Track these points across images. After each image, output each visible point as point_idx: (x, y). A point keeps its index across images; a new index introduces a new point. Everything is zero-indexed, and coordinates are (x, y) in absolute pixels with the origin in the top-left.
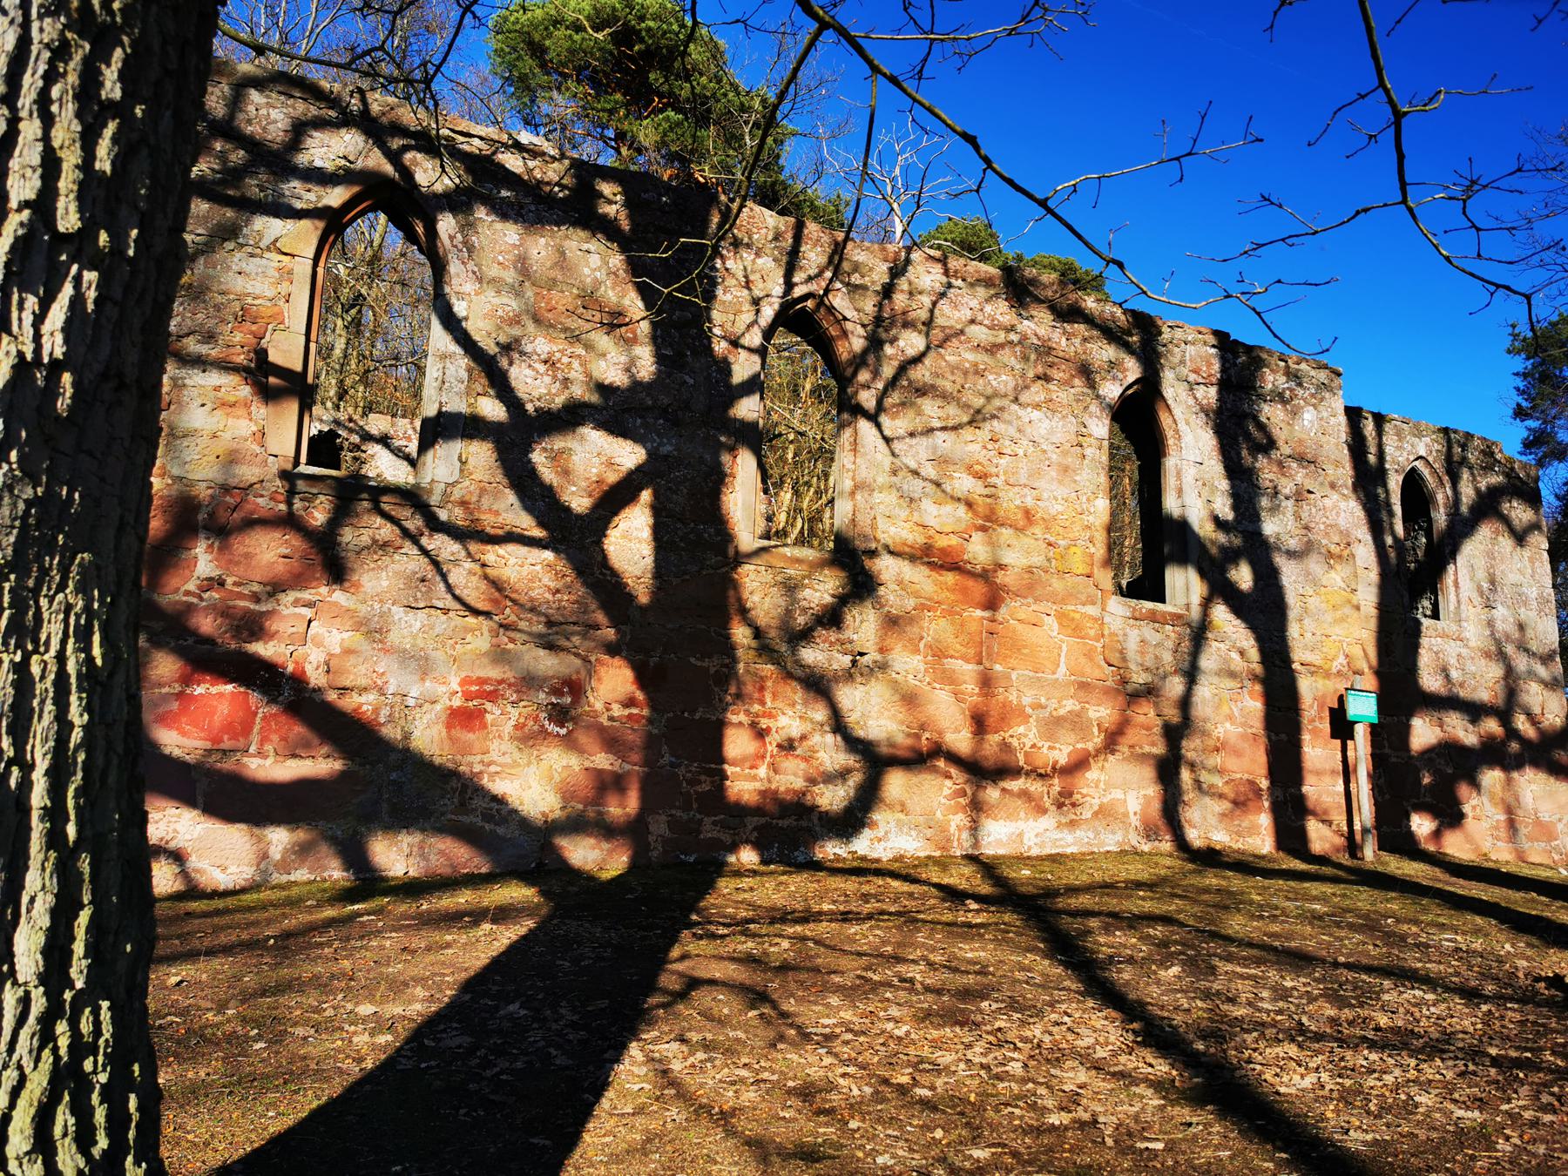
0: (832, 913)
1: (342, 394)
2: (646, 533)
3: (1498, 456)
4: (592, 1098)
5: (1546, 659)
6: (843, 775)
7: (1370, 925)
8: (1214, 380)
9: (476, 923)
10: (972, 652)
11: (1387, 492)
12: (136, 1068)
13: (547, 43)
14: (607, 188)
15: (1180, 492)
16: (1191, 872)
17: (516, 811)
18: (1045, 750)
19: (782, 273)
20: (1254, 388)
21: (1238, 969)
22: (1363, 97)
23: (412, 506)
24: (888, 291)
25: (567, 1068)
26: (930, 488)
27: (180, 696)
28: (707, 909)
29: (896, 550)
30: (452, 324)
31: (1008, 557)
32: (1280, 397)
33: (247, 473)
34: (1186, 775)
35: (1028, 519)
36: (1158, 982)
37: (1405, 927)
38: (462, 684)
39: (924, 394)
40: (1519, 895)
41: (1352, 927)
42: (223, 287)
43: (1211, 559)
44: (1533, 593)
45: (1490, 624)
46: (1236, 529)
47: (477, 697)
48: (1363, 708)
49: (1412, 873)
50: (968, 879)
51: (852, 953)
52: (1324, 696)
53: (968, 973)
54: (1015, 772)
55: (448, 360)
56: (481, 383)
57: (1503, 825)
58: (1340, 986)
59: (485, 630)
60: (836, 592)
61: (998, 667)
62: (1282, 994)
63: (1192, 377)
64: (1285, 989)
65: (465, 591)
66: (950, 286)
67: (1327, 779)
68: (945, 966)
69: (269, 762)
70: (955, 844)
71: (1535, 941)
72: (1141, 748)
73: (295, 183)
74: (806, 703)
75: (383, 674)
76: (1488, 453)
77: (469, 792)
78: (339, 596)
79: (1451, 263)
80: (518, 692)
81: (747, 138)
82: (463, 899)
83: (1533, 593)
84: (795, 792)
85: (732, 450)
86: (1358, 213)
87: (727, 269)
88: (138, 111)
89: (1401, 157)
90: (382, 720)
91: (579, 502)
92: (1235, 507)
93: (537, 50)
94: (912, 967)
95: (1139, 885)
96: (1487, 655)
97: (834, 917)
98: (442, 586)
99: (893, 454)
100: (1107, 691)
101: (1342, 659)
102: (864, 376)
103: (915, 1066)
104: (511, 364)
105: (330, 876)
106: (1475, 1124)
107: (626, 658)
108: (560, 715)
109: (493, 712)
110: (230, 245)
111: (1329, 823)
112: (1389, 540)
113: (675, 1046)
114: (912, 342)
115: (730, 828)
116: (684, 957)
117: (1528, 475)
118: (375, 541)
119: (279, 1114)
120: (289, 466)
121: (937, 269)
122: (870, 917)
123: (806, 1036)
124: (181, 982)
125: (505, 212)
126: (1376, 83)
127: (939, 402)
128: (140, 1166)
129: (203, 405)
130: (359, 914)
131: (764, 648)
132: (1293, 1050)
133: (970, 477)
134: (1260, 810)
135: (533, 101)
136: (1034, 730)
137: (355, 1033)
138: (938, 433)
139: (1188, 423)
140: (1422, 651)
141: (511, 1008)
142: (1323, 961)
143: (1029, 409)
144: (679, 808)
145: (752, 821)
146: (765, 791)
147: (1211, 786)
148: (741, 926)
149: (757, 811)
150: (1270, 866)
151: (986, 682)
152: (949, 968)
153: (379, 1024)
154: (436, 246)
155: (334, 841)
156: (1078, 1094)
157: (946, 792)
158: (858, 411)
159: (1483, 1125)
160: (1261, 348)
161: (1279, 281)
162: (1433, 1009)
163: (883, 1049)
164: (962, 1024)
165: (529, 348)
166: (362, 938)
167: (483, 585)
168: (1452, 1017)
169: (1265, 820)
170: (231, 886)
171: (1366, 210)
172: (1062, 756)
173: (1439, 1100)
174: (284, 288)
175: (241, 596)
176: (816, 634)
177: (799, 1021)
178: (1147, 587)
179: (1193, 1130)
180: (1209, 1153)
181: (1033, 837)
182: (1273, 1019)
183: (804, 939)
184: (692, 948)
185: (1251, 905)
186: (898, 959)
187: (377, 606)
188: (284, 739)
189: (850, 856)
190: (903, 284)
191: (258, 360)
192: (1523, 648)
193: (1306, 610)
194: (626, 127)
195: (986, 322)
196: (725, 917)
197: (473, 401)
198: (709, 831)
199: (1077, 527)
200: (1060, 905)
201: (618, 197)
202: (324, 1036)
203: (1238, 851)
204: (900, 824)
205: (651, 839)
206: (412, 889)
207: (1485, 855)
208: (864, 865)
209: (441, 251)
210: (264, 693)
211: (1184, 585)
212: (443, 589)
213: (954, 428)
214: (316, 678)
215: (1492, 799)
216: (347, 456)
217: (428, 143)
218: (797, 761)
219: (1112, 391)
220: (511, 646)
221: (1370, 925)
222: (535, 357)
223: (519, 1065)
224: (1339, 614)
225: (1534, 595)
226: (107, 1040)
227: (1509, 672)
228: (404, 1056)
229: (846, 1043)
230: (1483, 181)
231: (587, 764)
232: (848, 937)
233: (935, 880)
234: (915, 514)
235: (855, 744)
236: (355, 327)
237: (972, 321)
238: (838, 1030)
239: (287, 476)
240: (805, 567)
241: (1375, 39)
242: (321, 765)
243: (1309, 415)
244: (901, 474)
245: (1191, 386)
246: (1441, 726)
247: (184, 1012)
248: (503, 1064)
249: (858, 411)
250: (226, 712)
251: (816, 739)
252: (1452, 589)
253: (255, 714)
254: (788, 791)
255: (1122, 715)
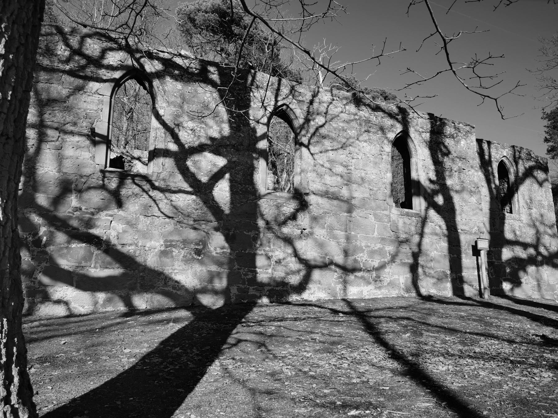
0: (291, 318)
1: (127, 143)
2: (228, 189)
3: (533, 155)
4: (200, 377)
5: (551, 227)
6: (299, 271)
7: (480, 320)
8: (429, 131)
9: (168, 323)
10: (343, 228)
11: (492, 169)
12: (16, 339)
13: (196, 17)
14: (212, 69)
15: (417, 170)
16: (421, 303)
17: (184, 286)
18: (370, 262)
19: (274, 97)
20: (443, 133)
21: (431, 334)
22: (432, 35)
23: (146, 181)
24: (311, 102)
25: (193, 368)
26: (328, 171)
27: (67, 248)
28: (248, 317)
29: (316, 193)
30: (158, 117)
31: (356, 194)
32: (452, 136)
33: (87, 171)
34: (420, 270)
35: (363, 181)
36: (401, 339)
37: (493, 320)
38: (164, 242)
39: (325, 138)
40: (534, 309)
41: (474, 320)
42: (79, 107)
43: (429, 194)
44: (546, 203)
45: (530, 215)
46: (437, 183)
47: (170, 247)
48: (484, 245)
49: (501, 302)
50: (342, 307)
51: (296, 331)
52: (470, 241)
53: (335, 336)
54: (360, 270)
55: (158, 130)
56: (169, 138)
57: (536, 286)
58: (466, 339)
59: (172, 223)
60: (295, 208)
61: (353, 233)
62: (444, 342)
63: (421, 130)
64: (446, 340)
65: (165, 210)
66: (333, 100)
67: (471, 270)
68: (328, 335)
69: (98, 270)
70: (339, 295)
71: (539, 324)
72: (404, 260)
73: (103, 70)
74: (285, 246)
75: (137, 239)
76: (529, 154)
77: (167, 279)
78: (121, 213)
79: (468, 89)
80: (184, 244)
81: (266, 49)
82: (165, 315)
83: (546, 203)
84: (282, 278)
85: (257, 159)
86: (438, 73)
87: (254, 96)
88: (11, 56)
89: (447, 54)
90: (137, 255)
91: (204, 179)
92: (437, 175)
93: (192, 20)
94: (316, 335)
95: (401, 308)
96: (529, 225)
97: (291, 319)
98: (157, 208)
99: (314, 159)
100: (392, 241)
101: (476, 228)
102: (303, 132)
103: (311, 366)
104: (179, 131)
105: (120, 309)
106: (498, 381)
107: (221, 232)
108: (198, 252)
109: (175, 252)
110: (81, 92)
111: (471, 286)
112: (493, 186)
113: (231, 361)
114: (320, 120)
115: (259, 291)
116: (237, 333)
117: (543, 162)
118: (133, 193)
119: (94, 383)
120: (103, 168)
121: (329, 94)
122: (304, 319)
123: (275, 357)
124: (65, 343)
125: (176, 78)
126: (436, 30)
127: (331, 141)
128: (17, 368)
129: (73, 148)
130: (128, 321)
131: (268, 227)
132: (442, 359)
133: (342, 167)
134: (447, 281)
135: (191, 38)
136: (366, 255)
137: (123, 358)
138: (330, 151)
139: (419, 146)
140: (506, 225)
141: (176, 349)
142: (461, 332)
143: (363, 142)
144: (241, 284)
145: (267, 288)
146: (271, 278)
147: (430, 273)
148: (259, 323)
149: (269, 285)
150: (450, 301)
151: (348, 238)
152: (329, 335)
153: (131, 356)
154: (153, 91)
155: (121, 297)
156: (364, 373)
157: (335, 277)
158: (302, 144)
159: (500, 381)
160: (445, 119)
161: (418, 96)
162: (496, 346)
163: (302, 360)
164: (330, 353)
165: (185, 125)
166: (128, 328)
167: (171, 208)
168: (502, 348)
169: (449, 285)
170: (86, 313)
171: (440, 72)
172: (376, 264)
173: (488, 373)
174: (100, 106)
175: (87, 213)
176: (288, 222)
177: (274, 352)
178: (407, 204)
179: (401, 383)
180: (404, 390)
181: (366, 292)
182: (439, 350)
183: (280, 326)
184: (240, 330)
185: (439, 313)
186: (312, 332)
187: (134, 216)
188: (103, 262)
189: (301, 300)
190: (317, 100)
191: (91, 131)
192: (542, 223)
193: (463, 211)
194: (224, 46)
195: (347, 112)
196: (254, 320)
197: (166, 144)
198: (252, 292)
199: (380, 184)
200: (372, 315)
201: (216, 72)
202: (112, 359)
203: (439, 296)
204: (319, 288)
205: (231, 295)
206: (147, 313)
207: (530, 296)
208: (306, 303)
209: (154, 92)
210: (96, 246)
211: (419, 203)
212: (157, 209)
213: (336, 150)
214: (114, 241)
215: (532, 277)
216: (126, 164)
217: (150, 56)
218: (282, 267)
219: (392, 136)
220: (181, 229)
221: (480, 320)
222: (188, 128)
223: (177, 367)
224: (475, 212)
225: (546, 204)
226: (5, 330)
227: (538, 232)
228: (138, 365)
229: (289, 359)
230: (479, 61)
231: (208, 269)
232: (296, 326)
233: (330, 307)
234: (323, 180)
235: (301, 261)
236: (131, 119)
237: (342, 112)
238: (287, 355)
239: (103, 172)
240: (284, 199)
241: (433, 16)
242: (115, 271)
243: (463, 142)
244: (317, 166)
245: (420, 133)
246: (513, 251)
247: (65, 353)
248: (172, 367)
249: (302, 144)
250: (83, 253)
251: (289, 259)
252: (517, 203)
253: (93, 253)
254: (279, 277)
255: (397, 249)
